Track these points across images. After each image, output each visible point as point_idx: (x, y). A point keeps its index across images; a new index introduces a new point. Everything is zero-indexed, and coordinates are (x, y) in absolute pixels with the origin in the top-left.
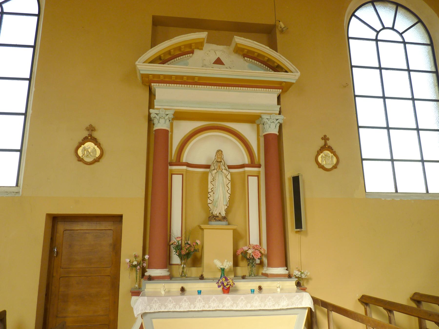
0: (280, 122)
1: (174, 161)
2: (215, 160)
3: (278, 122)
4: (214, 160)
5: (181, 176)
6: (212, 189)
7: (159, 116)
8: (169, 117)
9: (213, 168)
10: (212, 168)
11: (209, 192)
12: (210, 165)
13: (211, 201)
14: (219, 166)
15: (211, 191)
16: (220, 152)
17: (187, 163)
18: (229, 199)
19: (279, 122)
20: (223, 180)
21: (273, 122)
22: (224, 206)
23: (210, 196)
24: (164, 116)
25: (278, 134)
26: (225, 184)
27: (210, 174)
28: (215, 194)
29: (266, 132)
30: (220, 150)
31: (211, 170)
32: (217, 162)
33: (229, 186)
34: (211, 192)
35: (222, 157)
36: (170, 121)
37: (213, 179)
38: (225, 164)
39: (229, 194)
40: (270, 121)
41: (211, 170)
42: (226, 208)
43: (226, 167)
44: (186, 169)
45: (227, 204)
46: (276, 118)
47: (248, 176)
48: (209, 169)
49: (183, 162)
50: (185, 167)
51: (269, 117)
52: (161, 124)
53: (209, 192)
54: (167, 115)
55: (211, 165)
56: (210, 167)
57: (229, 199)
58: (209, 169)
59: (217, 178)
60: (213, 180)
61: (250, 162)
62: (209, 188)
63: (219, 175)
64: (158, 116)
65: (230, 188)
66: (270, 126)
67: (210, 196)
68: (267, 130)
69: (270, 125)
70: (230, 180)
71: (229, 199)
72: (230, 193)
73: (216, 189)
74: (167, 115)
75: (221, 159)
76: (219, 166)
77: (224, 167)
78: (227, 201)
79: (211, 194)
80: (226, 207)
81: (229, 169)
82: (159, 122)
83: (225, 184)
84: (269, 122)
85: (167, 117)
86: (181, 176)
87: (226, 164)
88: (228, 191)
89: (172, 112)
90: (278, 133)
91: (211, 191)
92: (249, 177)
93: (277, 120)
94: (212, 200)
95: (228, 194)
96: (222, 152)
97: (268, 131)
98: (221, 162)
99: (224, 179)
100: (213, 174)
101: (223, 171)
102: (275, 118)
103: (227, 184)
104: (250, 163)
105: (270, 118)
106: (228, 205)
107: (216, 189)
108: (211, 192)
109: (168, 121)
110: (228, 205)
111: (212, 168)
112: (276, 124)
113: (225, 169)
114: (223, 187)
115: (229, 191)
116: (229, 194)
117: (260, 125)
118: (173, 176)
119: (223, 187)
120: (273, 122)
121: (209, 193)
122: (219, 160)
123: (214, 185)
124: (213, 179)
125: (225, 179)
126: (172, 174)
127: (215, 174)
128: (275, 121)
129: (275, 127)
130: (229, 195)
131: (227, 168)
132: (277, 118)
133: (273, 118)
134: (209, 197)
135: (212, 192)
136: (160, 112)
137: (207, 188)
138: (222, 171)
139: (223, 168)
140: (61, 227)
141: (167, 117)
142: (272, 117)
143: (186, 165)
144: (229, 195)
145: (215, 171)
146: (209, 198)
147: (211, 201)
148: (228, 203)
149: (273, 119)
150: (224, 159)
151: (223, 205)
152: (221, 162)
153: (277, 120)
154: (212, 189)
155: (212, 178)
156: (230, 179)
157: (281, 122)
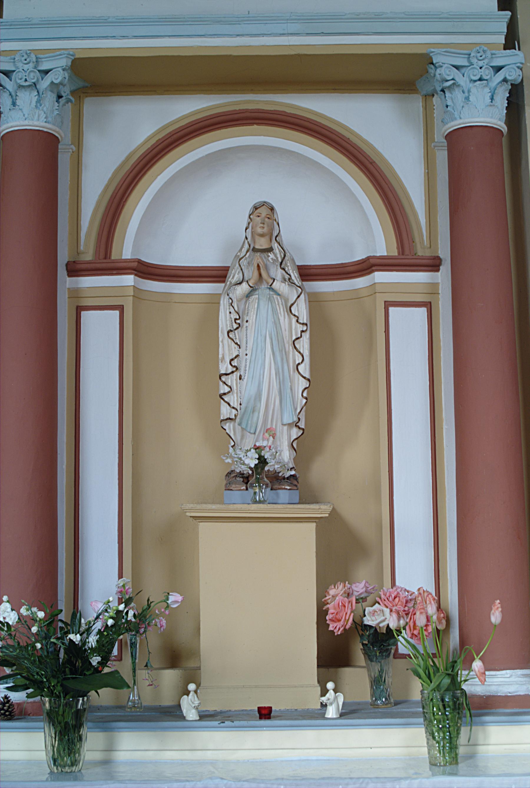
0: (509, 78)
1: (89, 256)
2: (246, 246)
3: (501, 78)
4: (244, 242)
5: (117, 313)
6: (232, 360)
7: (13, 80)
8: (52, 83)
9: (236, 276)
10: (233, 278)
11: (223, 372)
12: (226, 269)
13: (233, 408)
14: (258, 266)
15: (230, 369)
16: (264, 211)
17: (139, 262)
18: (305, 401)
19: (505, 80)
20: (277, 323)
21: (480, 79)
22: (285, 428)
23: (227, 389)
24: (33, 77)
25: (504, 129)
26: (286, 334)
27: (224, 302)
28: (245, 380)
29: (453, 123)
30: (264, 204)
31: (231, 283)
32: (255, 250)
33: (304, 345)
34: (233, 372)
35: (272, 230)
36: (60, 97)
37: (238, 321)
38: (286, 258)
39: (304, 378)
40: (469, 77)
41: (231, 283)
42: (295, 437)
43: (291, 272)
44: (134, 286)
45: (296, 419)
46: (492, 65)
47: (388, 305)
48: (223, 285)
49: (124, 257)
50: (129, 280)
51: (461, 61)
52: (24, 111)
53: (220, 376)
54: (47, 72)
55: (229, 267)
56: (226, 277)
57: (306, 398)
58: (224, 282)
59: (252, 317)
60: (235, 326)
61: (396, 251)
62: (220, 356)
63: (262, 303)
64: (11, 80)
65: (306, 353)
66: (469, 95)
67: (227, 389)
68: (456, 113)
69: (469, 91)
70: (305, 322)
71: (305, 401)
72: (307, 376)
73: (248, 361)
74: (47, 72)
75: (271, 241)
76: (258, 266)
77: (280, 271)
78: (296, 409)
79: (231, 380)
80: (295, 433)
81: (303, 280)
82: (14, 104)
83: (286, 334)
84: (462, 81)
85: (44, 84)
86: (117, 313)
87: (293, 260)
88: (299, 367)
89: (65, 62)
90: (505, 123)
91: (230, 369)
92: (391, 309)
93: (498, 69)
94: (235, 406)
95: (301, 378)
96: (272, 209)
97: (461, 118)
98: (270, 250)
99: (282, 319)
100: (235, 300)
101: (276, 285)
102: (486, 61)
103: (294, 338)
104: (395, 253)
105: (469, 61)
106: (302, 425)
107: (248, 361)
108: (233, 372)
109: (51, 97)
110: (302, 425)
111: (234, 276)
112: (495, 89)
113: (287, 277)
114: (277, 354)
115: (305, 369)
116: (304, 378)
117: (434, 99)
118: (83, 313)
119: (277, 354)
120: (480, 79)
121: (220, 376)
122: (262, 243)
123: (243, 346)
124: (238, 321)
125: (284, 320)
126: (79, 309)
127: (246, 302)
128: (487, 73)
129: (492, 99)
130: (306, 384)
131: (295, 276)
132: (497, 62)
133: (481, 63)
134: (225, 394)
135: (236, 375)
136: (20, 65)
137: (216, 360)
138: (271, 288)
139: (279, 273)
140: (120, 659)
141: (44, 84)
142: (474, 61)
143: (135, 270)
144: (306, 384)
145: (245, 286)
146: (226, 398)
147: (233, 408)
148: (302, 416)
149: (481, 66)
150: (285, 237)
151: (279, 424)
152: (270, 250)
153: (498, 69)
154: (232, 360)
155: (232, 316)
156: (304, 318)
157: (514, 75)
